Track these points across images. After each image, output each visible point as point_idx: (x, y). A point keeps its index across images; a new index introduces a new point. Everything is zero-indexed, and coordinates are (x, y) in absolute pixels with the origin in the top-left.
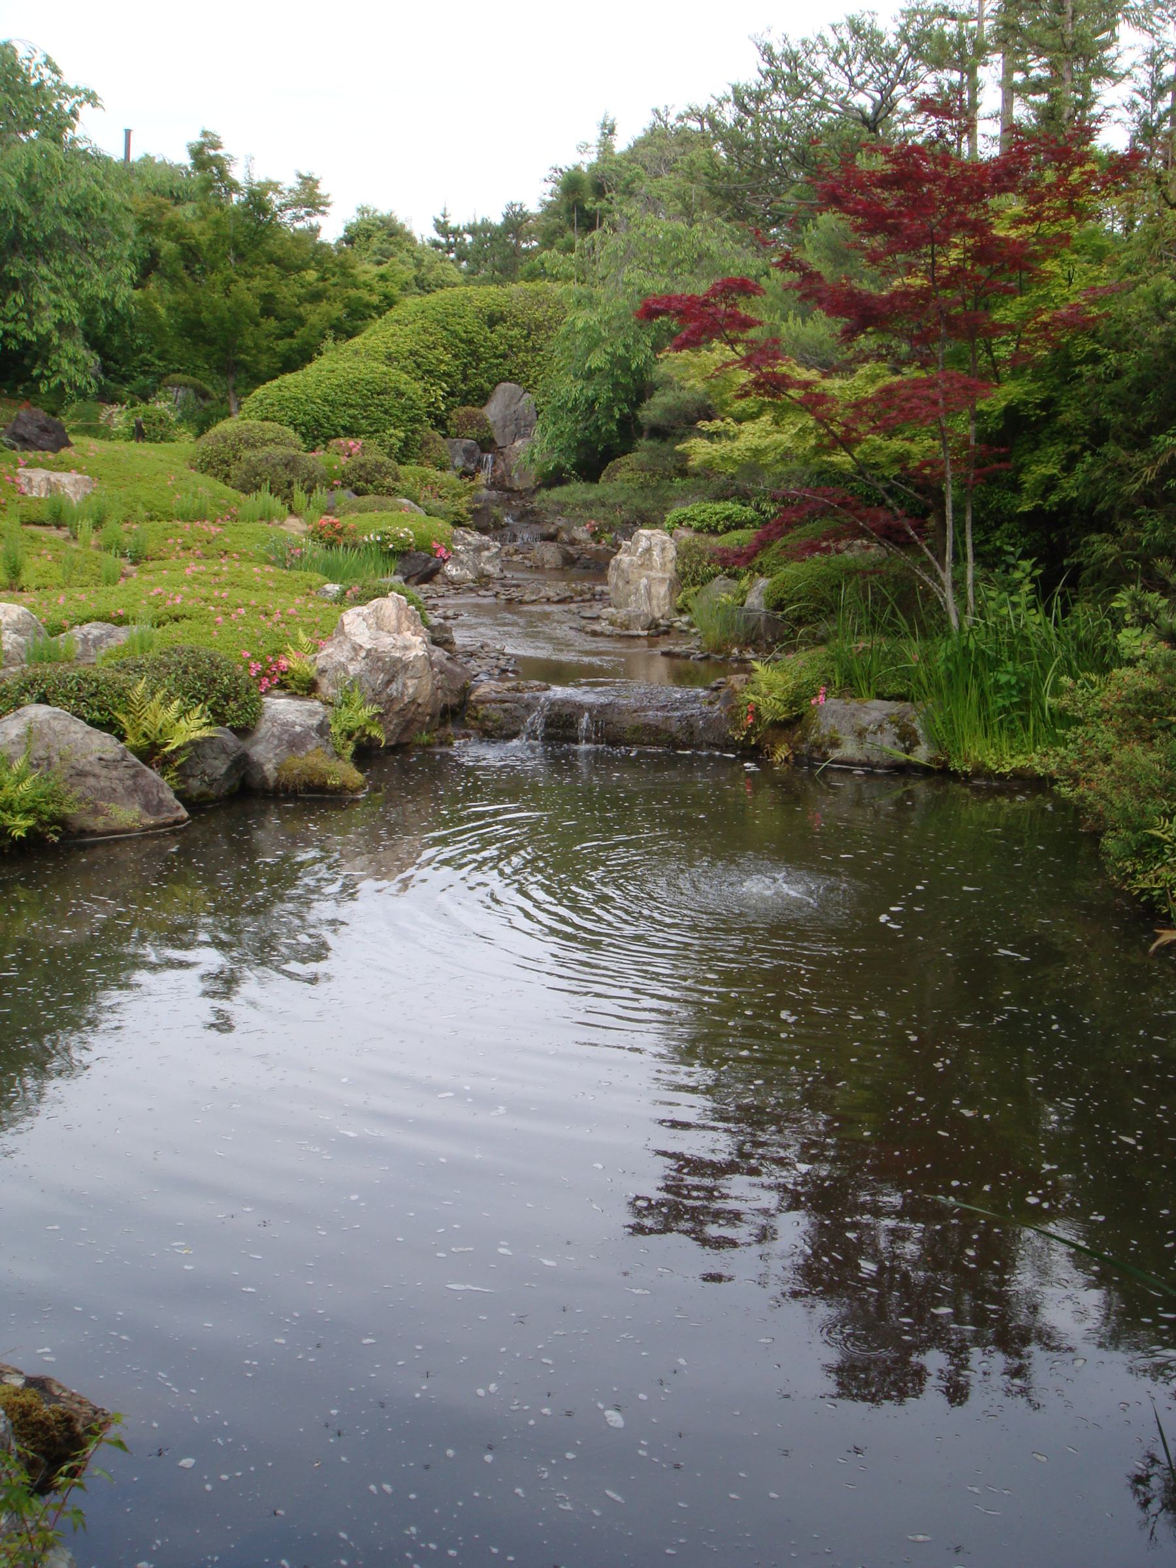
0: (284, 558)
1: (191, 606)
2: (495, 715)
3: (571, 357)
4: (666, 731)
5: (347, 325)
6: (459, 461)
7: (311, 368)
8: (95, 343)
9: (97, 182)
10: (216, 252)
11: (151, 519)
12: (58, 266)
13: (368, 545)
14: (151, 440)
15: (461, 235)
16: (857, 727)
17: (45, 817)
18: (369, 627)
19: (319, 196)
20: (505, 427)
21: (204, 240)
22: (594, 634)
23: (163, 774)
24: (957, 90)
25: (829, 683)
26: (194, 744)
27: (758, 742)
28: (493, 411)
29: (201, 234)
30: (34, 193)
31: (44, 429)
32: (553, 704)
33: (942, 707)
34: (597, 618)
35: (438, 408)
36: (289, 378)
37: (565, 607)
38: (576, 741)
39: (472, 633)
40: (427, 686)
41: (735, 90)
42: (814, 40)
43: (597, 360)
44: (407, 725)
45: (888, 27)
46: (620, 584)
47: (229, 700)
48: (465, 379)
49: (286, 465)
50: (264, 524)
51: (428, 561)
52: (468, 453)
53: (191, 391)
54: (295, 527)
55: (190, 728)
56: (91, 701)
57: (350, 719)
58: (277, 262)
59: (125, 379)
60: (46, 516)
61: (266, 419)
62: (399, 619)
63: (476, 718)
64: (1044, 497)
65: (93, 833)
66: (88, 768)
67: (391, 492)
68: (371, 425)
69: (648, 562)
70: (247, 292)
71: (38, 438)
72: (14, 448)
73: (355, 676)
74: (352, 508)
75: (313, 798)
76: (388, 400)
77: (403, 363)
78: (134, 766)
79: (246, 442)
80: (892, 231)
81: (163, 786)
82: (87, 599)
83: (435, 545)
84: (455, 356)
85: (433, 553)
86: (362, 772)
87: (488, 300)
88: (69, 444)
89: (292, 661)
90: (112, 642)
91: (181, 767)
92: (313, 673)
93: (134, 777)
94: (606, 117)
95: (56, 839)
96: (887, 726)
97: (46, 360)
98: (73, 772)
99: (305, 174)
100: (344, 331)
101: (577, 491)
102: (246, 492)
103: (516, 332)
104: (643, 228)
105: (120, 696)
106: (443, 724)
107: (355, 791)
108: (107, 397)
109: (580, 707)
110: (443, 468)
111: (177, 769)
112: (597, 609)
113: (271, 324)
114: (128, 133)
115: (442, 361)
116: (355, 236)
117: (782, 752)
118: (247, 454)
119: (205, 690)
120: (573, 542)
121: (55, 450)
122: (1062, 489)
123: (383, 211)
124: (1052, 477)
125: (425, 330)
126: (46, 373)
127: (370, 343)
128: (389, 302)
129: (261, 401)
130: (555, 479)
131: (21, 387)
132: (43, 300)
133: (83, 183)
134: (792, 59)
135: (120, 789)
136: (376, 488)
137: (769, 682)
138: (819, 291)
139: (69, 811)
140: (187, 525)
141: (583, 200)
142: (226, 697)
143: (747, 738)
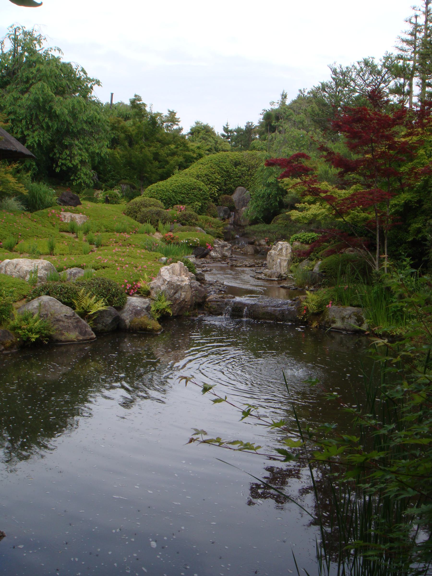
0: (151, 247)
1: (111, 263)
2: (214, 307)
3: (263, 178)
5: (185, 164)
6: (222, 214)
7: (169, 179)
8: (94, 168)
9: (97, 112)
10: (138, 137)
11: (107, 231)
12: (82, 141)
13: (183, 244)
14: (111, 203)
15: (233, 132)
16: (342, 316)
17: (43, 335)
18: (169, 273)
19: (176, 119)
21: (134, 133)
22: (258, 279)
23: (88, 322)
24: (403, 85)
25: (333, 300)
26: (99, 311)
27: (307, 320)
28: (235, 197)
29: (133, 131)
30: (75, 115)
31: (72, 198)
32: (235, 303)
33: (372, 310)
34: (261, 273)
35: (215, 195)
36: (161, 183)
37: (251, 269)
38: (242, 317)
39: (215, 277)
40: (189, 295)
41: (322, 84)
42: (351, 67)
44: (181, 309)
45: (378, 62)
46: (271, 261)
47: (114, 296)
48: (225, 185)
49: (157, 214)
50: (146, 235)
51: (204, 250)
52: (225, 211)
53: (129, 186)
54: (158, 236)
55: (100, 306)
56: (65, 295)
57: (160, 306)
58: (159, 141)
59: (106, 181)
60: (69, 229)
61: (152, 197)
62: (180, 270)
63: (208, 307)
64: (416, 235)
65: (61, 341)
66: (61, 318)
67: (194, 225)
68: (189, 200)
69: (281, 254)
70: (149, 152)
72: (60, 205)
73: (163, 290)
74: (179, 230)
75: (142, 332)
76: (196, 192)
77: (203, 178)
78: (78, 318)
79: (144, 205)
80: (360, 138)
81: (87, 326)
82: (74, 259)
83: (207, 245)
84: (222, 177)
85: (206, 247)
86: (160, 324)
87: (235, 157)
88: (80, 204)
89: (141, 284)
90: (80, 275)
91: (95, 319)
92: (149, 289)
93: (77, 322)
94: (284, 92)
95: (47, 343)
96: (352, 316)
97: (76, 173)
98: (55, 319)
99: (171, 110)
100: (182, 167)
101: (262, 227)
102: (142, 222)
103: (244, 168)
104: (290, 133)
105: (75, 294)
106: (195, 309)
107: (157, 331)
108: (97, 187)
109: (245, 305)
110: (215, 217)
111: (93, 320)
112: (262, 270)
113: (157, 163)
114: (112, 94)
115: (217, 178)
116: (195, 132)
117: (315, 324)
118: (143, 209)
119: (106, 293)
120: (260, 245)
121: (75, 206)
122: (423, 232)
123: (205, 123)
124: (420, 228)
125: (211, 167)
126: (76, 178)
127: (191, 171)
128: (200, 156)
129: (150, 191)
130: (255, 222)
131: (67, 183)
132: (76, 153)
133: (92, 112)
134: (343, 74)
135: (71, 326)
136: (189, 223)
137: (311, 299)
138: (333, 159)
139: (51, 333)
140: (118, 234)
141: (272, 122)
142: (113, 296)
143: (303, 318)
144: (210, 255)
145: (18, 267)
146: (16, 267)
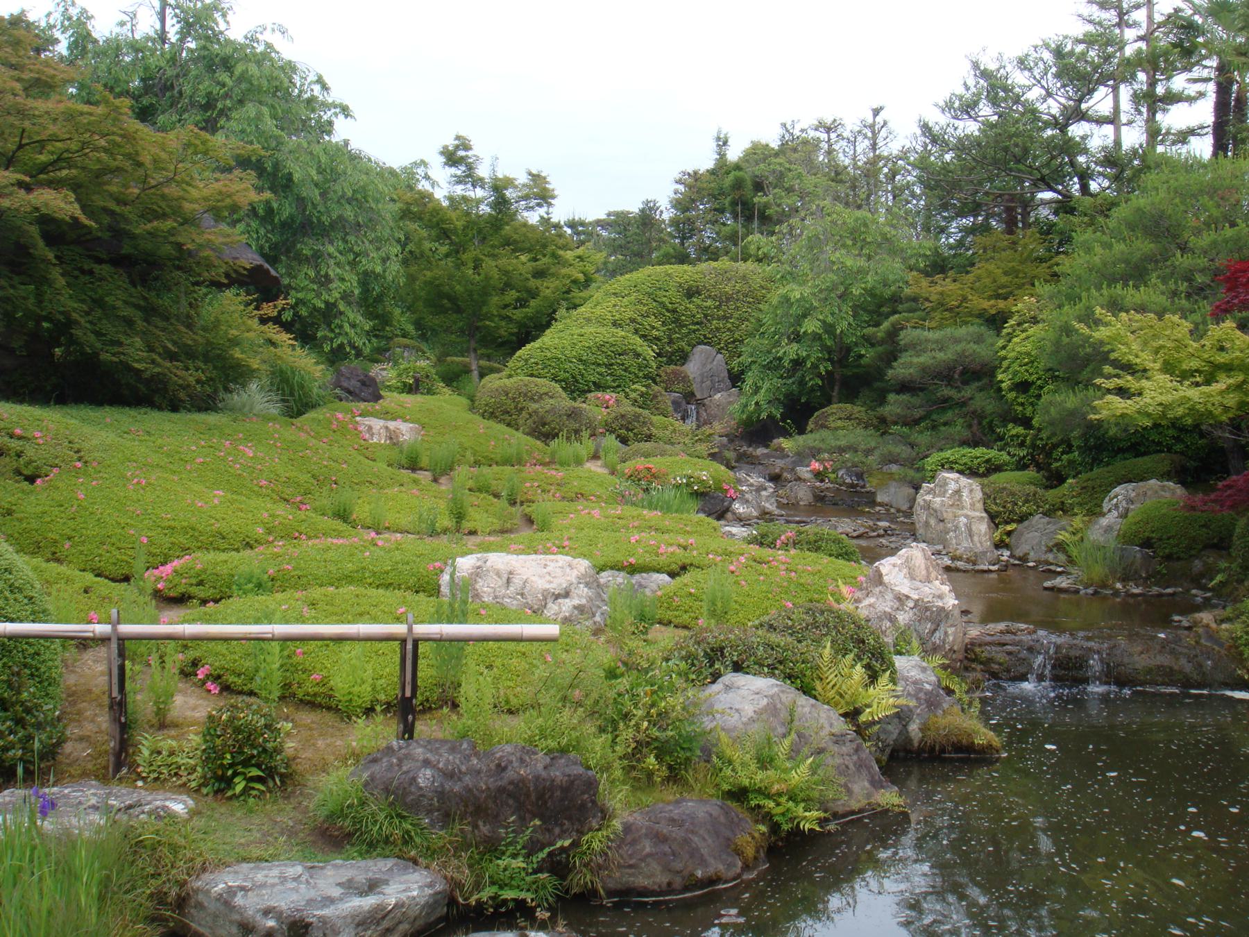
4: (1180, 672)
20: (702, 382)
28: (692, 368)
38: (1086, 681)
43: (810, 326)
46: (932, 522)
48: (671, 342)
62: (927, 569)
68: (614, 381)
71: (361, 391)
76: (628, 360)
84: (664, 324)
99: (534, 172)
103: (709, 303)
115: (653, 328)
144: (734, 514)
145: (517, 581)
146: (508, 581)
